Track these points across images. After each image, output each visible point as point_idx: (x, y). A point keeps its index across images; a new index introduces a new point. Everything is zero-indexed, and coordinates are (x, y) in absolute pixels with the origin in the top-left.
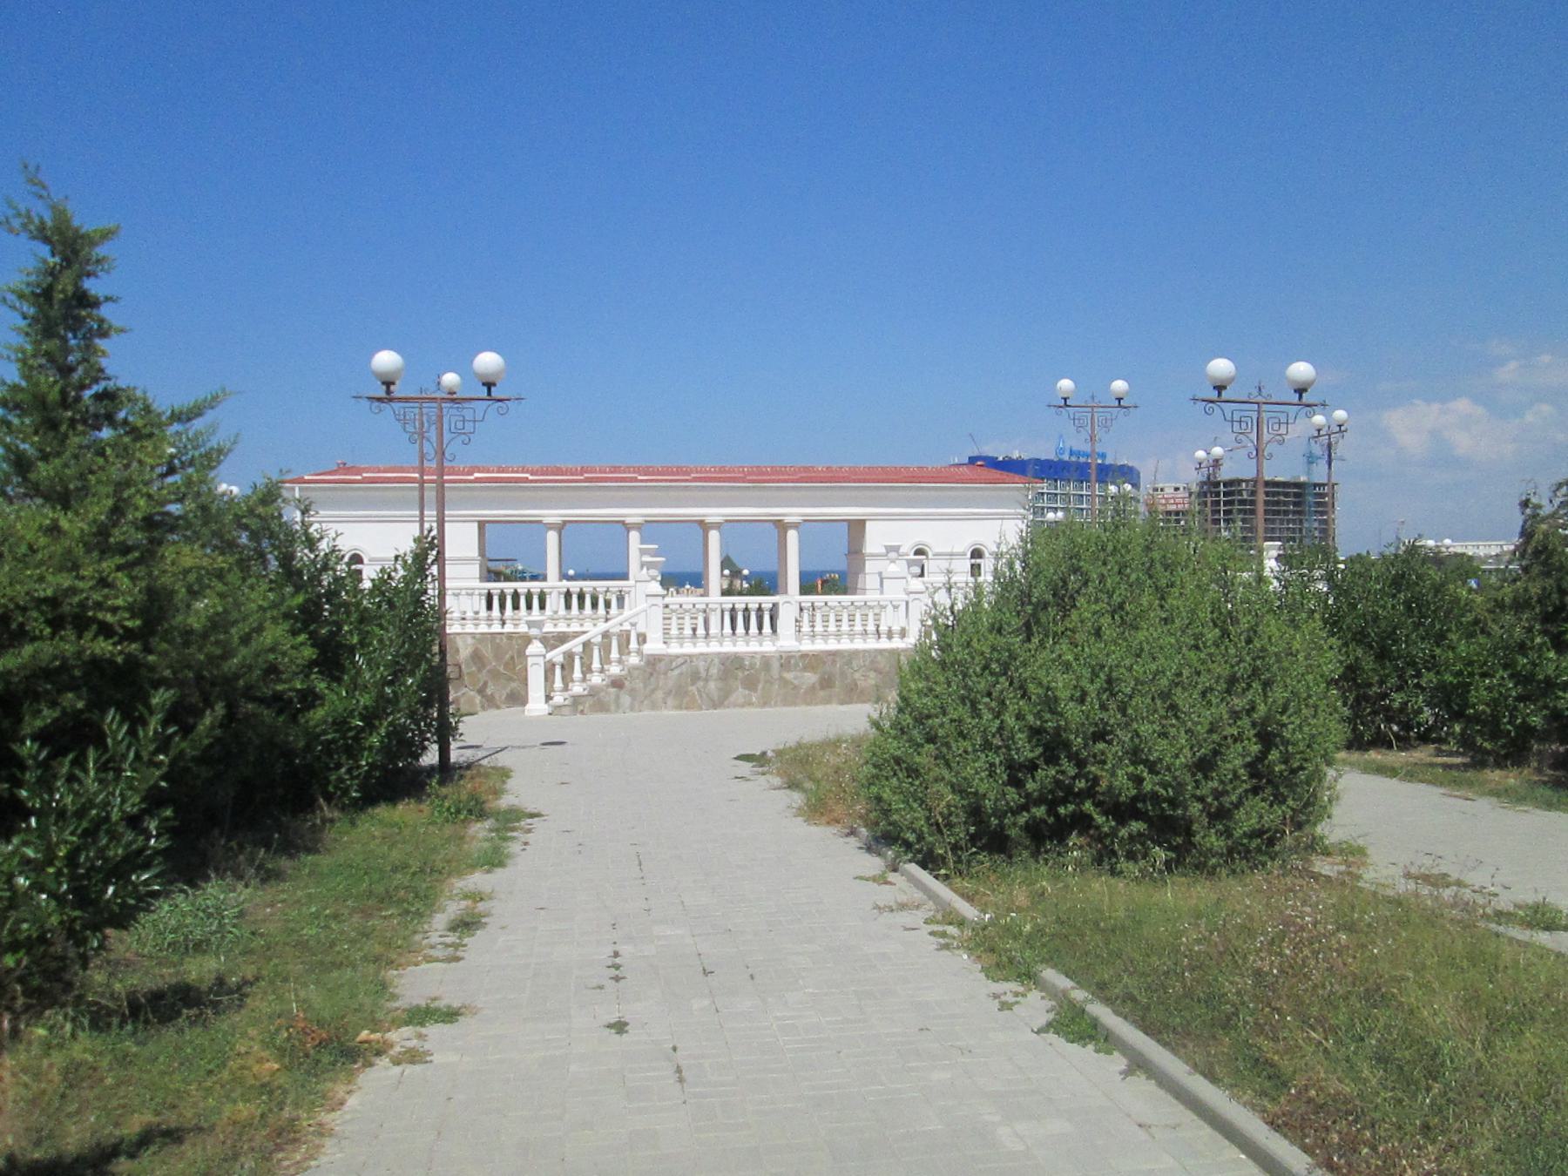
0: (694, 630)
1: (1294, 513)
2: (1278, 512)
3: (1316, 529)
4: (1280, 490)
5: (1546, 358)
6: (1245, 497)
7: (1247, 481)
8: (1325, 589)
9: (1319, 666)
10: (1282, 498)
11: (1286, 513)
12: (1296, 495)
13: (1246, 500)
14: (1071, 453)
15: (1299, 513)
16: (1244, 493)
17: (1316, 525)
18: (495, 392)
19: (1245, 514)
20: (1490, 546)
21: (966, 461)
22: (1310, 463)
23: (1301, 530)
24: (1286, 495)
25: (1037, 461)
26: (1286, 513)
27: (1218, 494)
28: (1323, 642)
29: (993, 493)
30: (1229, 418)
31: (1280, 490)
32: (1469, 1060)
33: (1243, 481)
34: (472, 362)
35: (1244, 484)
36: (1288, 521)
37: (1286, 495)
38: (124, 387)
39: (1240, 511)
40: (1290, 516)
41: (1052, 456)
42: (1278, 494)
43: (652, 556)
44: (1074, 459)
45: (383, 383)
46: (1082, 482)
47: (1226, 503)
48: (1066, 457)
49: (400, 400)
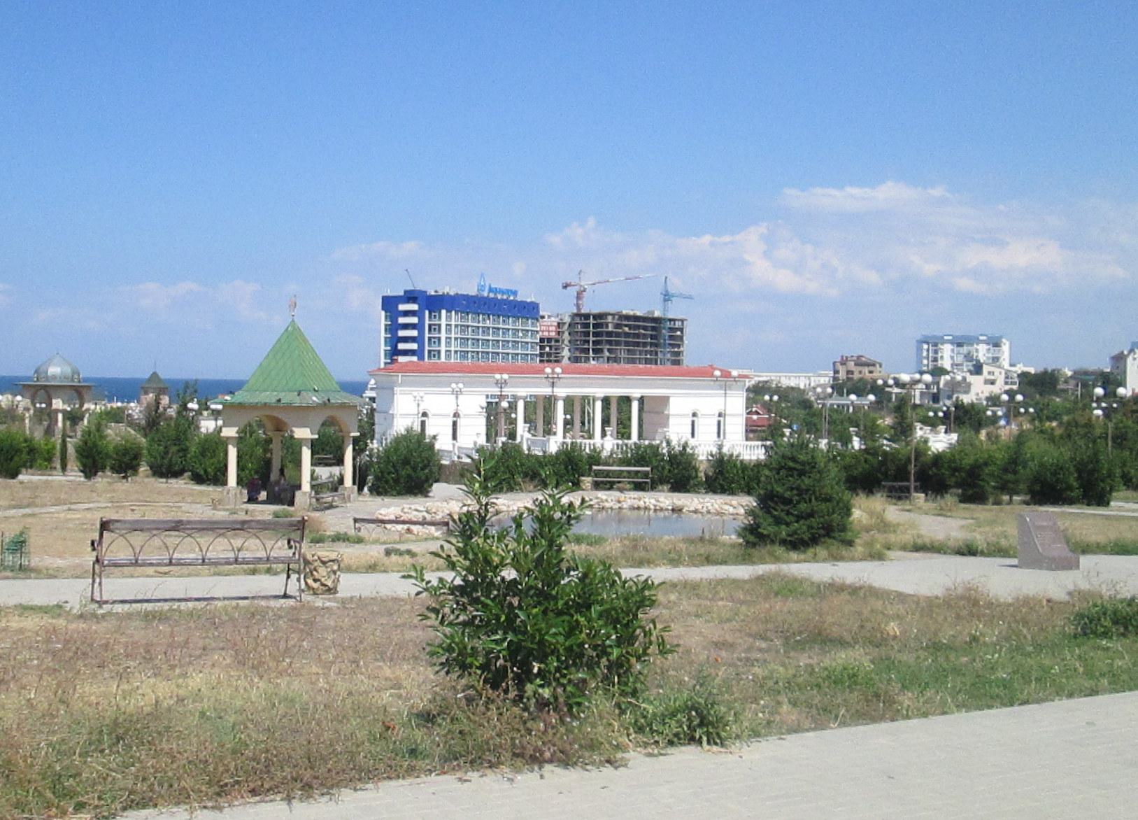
1: (651, 344)
2: (637, 344)
3: (668, 360)
4: (640, 324)
7: (613, 315)
8: (880, 422)
10: (626, 329)
11: (645, 344)
12: (653, 329)
13: (612, 332)
14: (491, 290)
15: (656, 345)
16: (610, 325)
19: (611, 345)
20: (799, 377)
22: (665, 300)
24: (645, 328)
26: (645, 344)
27: (587, 325)
29: (661, 382)
31: (640, 324)
33: (610, 314)
37: (645, 328)
40: (648, 348)
42: (638, 327)
43: (618, 466)
44: (492, 295)
47: (595, 334)
48: (485, 294)
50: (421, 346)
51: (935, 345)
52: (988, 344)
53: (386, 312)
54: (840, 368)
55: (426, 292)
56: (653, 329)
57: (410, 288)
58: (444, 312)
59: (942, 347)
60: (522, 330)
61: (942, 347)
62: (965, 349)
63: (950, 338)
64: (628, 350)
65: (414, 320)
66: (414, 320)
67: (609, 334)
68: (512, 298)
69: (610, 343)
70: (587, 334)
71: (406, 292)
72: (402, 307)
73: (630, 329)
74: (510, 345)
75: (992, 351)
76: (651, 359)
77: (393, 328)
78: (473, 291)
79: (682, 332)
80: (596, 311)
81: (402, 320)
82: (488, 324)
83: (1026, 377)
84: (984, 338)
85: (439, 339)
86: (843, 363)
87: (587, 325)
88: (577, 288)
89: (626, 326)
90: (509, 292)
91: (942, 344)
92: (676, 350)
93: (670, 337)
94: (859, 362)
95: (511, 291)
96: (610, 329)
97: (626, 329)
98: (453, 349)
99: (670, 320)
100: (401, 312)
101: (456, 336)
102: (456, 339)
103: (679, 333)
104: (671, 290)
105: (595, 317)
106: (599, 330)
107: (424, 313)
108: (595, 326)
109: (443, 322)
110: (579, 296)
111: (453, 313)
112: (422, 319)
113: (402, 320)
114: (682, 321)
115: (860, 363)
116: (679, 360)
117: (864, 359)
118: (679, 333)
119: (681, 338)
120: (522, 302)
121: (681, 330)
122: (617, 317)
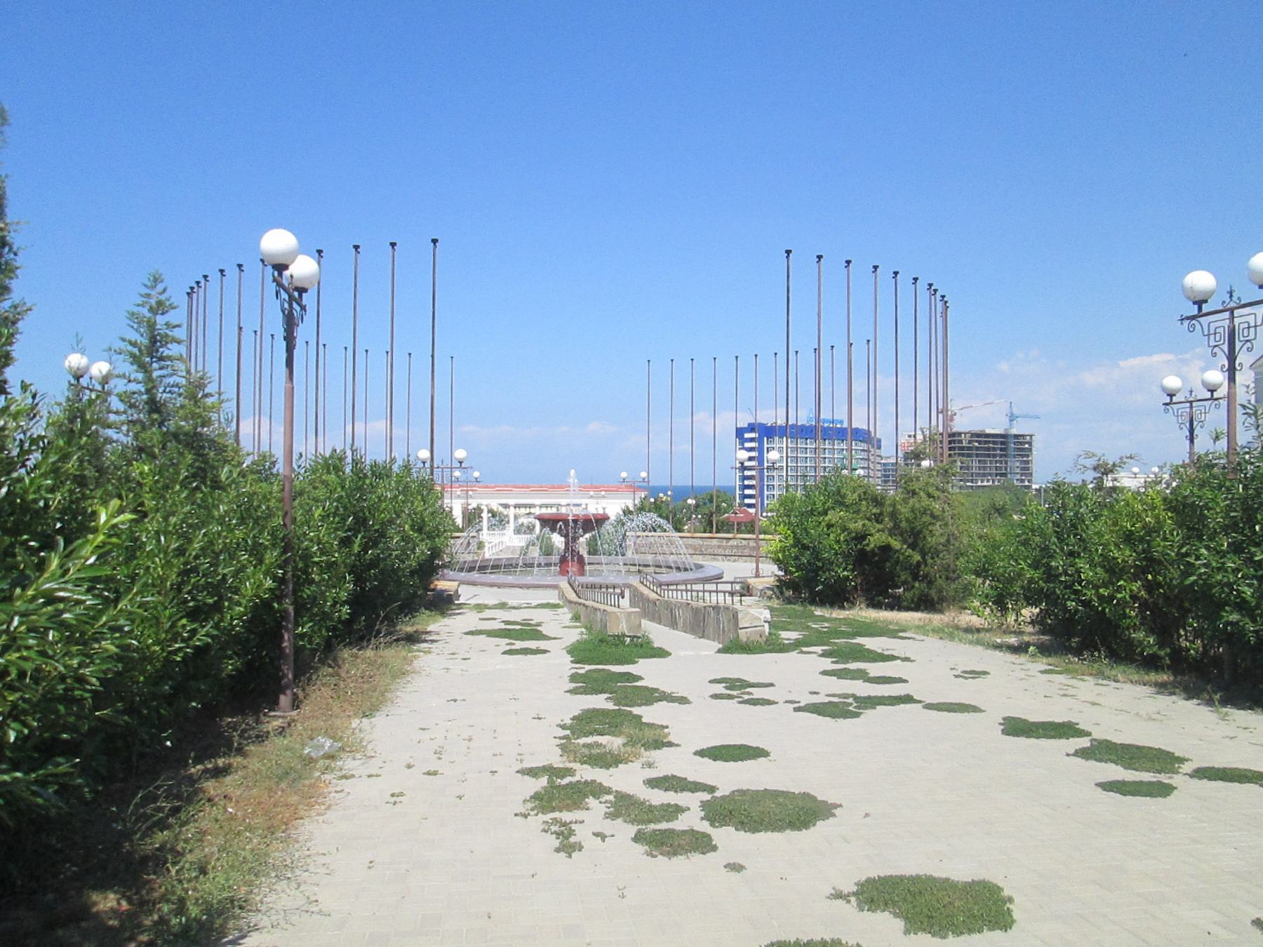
1: (1001, 456)
2: (989, 456)
6: (964, 445)
7: (965, 434)
9: (1092, 511)
10: (991, 445)
11: (995, 456)
12: (1002, 443)
15: (1005, 456)
17: (1018, 464)
18: (463, 465)
24: (994, 443)
26: (995, 456)
28: (318, 475)
30: (1206, 333)
32: (997, 558)
34: (1249, 259)
35: (963, 435)
37: (994, 443)
39: (959, 454)
40: (998, 459)
42: (989, 442)
45: (1195, 303)
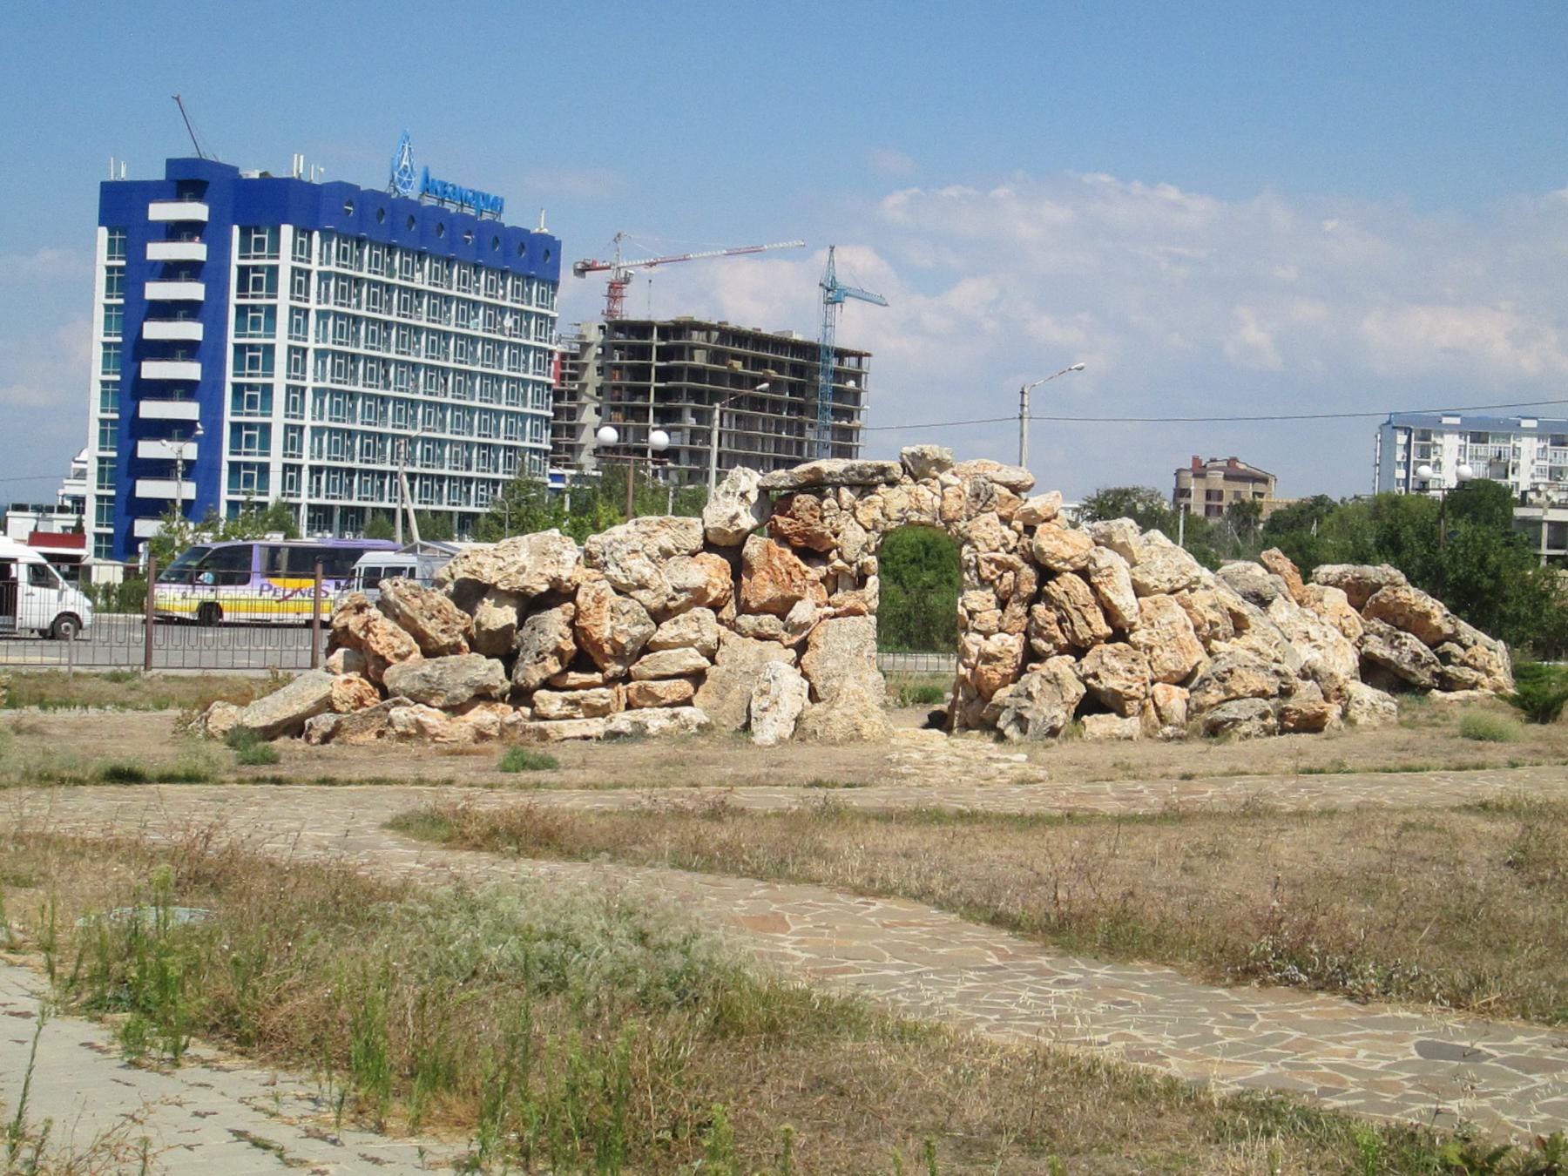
0: (1235, 773)
1: (792, 407)
5: (953, 192)
12: (797, 370)
15: (800, 409)
21: (1040, 527)
23: (800, 444)
24: (778, 366)
25: (344, 191)
36: (779, 424)
37: (778, 366)
38: (983, 924)
41: (382, 186)
44: (430, 201)
46: (360, 246)
47: (663, 374)
48: (413, 193)
49: (227, 625)
50: (216, 330)
51: (1425, 436)
52: (1540, 438)
53: (111, 232)
54: (1193, 485)
55: (235, 170)
56: (797, 370)
57: (186, 152)
58: (287, 231)
59: (1439, 441)
60: (514, 311)
61: (1439, 441)
62: (1490, 449)
63: (1457, 421)
64: (739, 418)
65: (195, 251)
66: (195, 251)
67: (697, 374)
68: (486, 216)
69: (697, 395)
70: (643, 373)
71: (172, 164)
72: (161, 212)
73: (745, 366)
74: (508, 322)
75: (1550, 455)
76: (789, 442)
77: (128, 279)
78: (373, 180)
79: (858, 384)
80: (663, 314)
81: (158, 251)
82: (420, 281)
83: (1206, 553)
84: (1533, 424)
85: (271, 311)
86: (1200, 471)
87: (644, 352)
88: (609, 275)
89: (736, 357)
90: (480, 198)
91: (1441, 434)
92: (844, 423)
93: (835, 390)
94: (1232, 472)
95: (485, 198)
96: (700, 360)
97: (738, 365)
98: (306, 461)
99: (841, 354)
100: (157, 224)
101: (316, 462)
102: (321, 354)
103: (851, 384)
104: (843, 280)
105: (665, 331)
106: (673, 363)
107: (231, 231)
108: (664, 354)
109: (285, 263)
110: (615, 290)
111: (316, 235)
112: (219, 250)
113: (158, 251)
114: (859, 356)
115: (1234, 474)
116: (851, 447)
117: (1242, 467)
118: (851, 384)
119: (856, 396)
120: (517, 231)
121: (857, 377)
122: (715, 334)
